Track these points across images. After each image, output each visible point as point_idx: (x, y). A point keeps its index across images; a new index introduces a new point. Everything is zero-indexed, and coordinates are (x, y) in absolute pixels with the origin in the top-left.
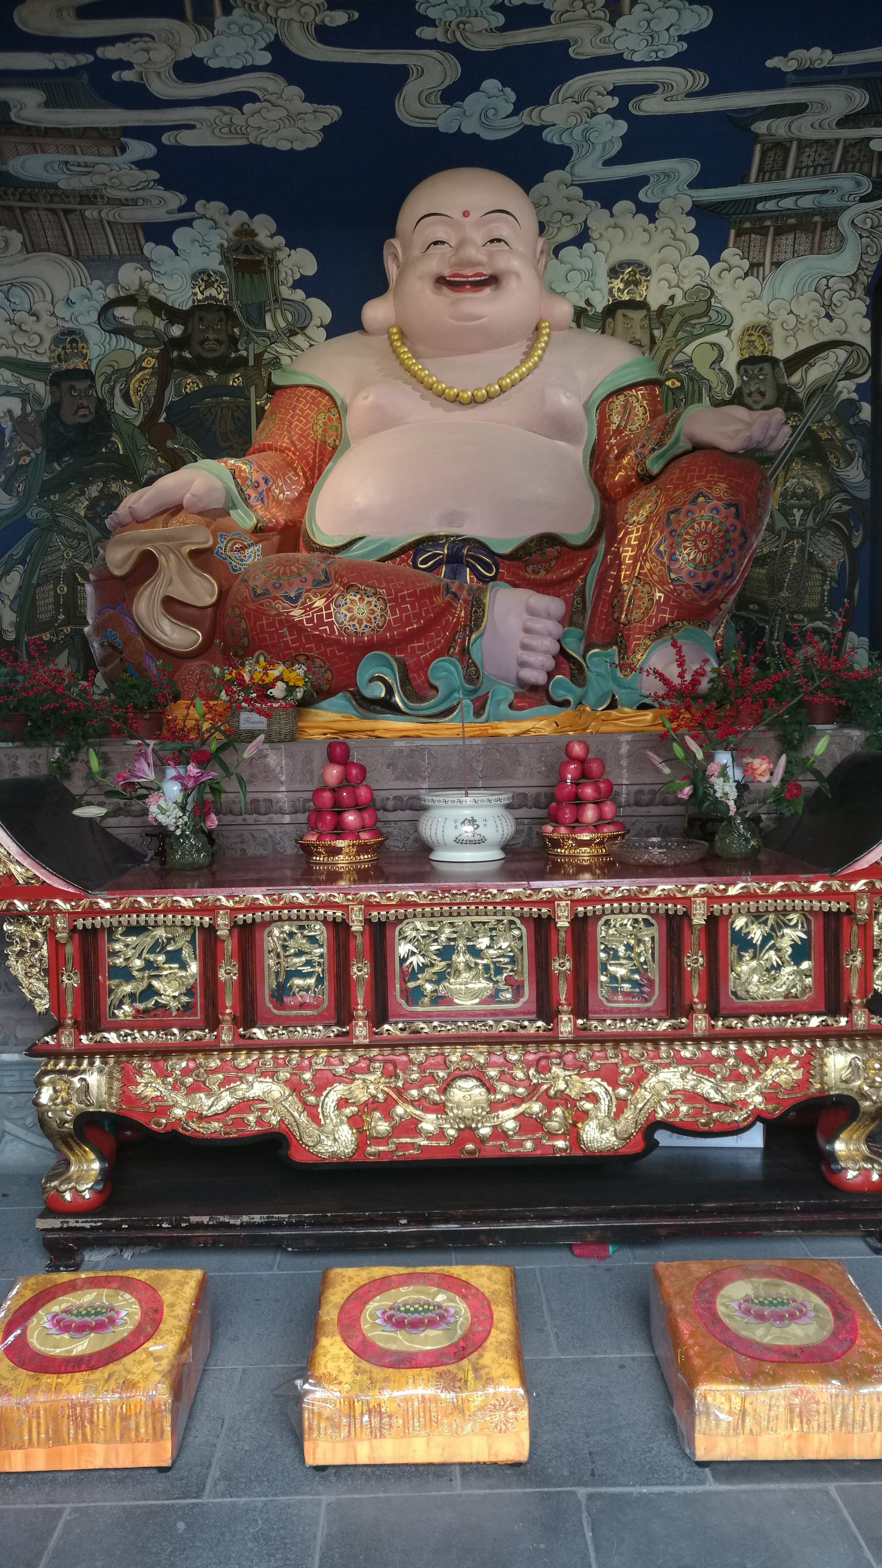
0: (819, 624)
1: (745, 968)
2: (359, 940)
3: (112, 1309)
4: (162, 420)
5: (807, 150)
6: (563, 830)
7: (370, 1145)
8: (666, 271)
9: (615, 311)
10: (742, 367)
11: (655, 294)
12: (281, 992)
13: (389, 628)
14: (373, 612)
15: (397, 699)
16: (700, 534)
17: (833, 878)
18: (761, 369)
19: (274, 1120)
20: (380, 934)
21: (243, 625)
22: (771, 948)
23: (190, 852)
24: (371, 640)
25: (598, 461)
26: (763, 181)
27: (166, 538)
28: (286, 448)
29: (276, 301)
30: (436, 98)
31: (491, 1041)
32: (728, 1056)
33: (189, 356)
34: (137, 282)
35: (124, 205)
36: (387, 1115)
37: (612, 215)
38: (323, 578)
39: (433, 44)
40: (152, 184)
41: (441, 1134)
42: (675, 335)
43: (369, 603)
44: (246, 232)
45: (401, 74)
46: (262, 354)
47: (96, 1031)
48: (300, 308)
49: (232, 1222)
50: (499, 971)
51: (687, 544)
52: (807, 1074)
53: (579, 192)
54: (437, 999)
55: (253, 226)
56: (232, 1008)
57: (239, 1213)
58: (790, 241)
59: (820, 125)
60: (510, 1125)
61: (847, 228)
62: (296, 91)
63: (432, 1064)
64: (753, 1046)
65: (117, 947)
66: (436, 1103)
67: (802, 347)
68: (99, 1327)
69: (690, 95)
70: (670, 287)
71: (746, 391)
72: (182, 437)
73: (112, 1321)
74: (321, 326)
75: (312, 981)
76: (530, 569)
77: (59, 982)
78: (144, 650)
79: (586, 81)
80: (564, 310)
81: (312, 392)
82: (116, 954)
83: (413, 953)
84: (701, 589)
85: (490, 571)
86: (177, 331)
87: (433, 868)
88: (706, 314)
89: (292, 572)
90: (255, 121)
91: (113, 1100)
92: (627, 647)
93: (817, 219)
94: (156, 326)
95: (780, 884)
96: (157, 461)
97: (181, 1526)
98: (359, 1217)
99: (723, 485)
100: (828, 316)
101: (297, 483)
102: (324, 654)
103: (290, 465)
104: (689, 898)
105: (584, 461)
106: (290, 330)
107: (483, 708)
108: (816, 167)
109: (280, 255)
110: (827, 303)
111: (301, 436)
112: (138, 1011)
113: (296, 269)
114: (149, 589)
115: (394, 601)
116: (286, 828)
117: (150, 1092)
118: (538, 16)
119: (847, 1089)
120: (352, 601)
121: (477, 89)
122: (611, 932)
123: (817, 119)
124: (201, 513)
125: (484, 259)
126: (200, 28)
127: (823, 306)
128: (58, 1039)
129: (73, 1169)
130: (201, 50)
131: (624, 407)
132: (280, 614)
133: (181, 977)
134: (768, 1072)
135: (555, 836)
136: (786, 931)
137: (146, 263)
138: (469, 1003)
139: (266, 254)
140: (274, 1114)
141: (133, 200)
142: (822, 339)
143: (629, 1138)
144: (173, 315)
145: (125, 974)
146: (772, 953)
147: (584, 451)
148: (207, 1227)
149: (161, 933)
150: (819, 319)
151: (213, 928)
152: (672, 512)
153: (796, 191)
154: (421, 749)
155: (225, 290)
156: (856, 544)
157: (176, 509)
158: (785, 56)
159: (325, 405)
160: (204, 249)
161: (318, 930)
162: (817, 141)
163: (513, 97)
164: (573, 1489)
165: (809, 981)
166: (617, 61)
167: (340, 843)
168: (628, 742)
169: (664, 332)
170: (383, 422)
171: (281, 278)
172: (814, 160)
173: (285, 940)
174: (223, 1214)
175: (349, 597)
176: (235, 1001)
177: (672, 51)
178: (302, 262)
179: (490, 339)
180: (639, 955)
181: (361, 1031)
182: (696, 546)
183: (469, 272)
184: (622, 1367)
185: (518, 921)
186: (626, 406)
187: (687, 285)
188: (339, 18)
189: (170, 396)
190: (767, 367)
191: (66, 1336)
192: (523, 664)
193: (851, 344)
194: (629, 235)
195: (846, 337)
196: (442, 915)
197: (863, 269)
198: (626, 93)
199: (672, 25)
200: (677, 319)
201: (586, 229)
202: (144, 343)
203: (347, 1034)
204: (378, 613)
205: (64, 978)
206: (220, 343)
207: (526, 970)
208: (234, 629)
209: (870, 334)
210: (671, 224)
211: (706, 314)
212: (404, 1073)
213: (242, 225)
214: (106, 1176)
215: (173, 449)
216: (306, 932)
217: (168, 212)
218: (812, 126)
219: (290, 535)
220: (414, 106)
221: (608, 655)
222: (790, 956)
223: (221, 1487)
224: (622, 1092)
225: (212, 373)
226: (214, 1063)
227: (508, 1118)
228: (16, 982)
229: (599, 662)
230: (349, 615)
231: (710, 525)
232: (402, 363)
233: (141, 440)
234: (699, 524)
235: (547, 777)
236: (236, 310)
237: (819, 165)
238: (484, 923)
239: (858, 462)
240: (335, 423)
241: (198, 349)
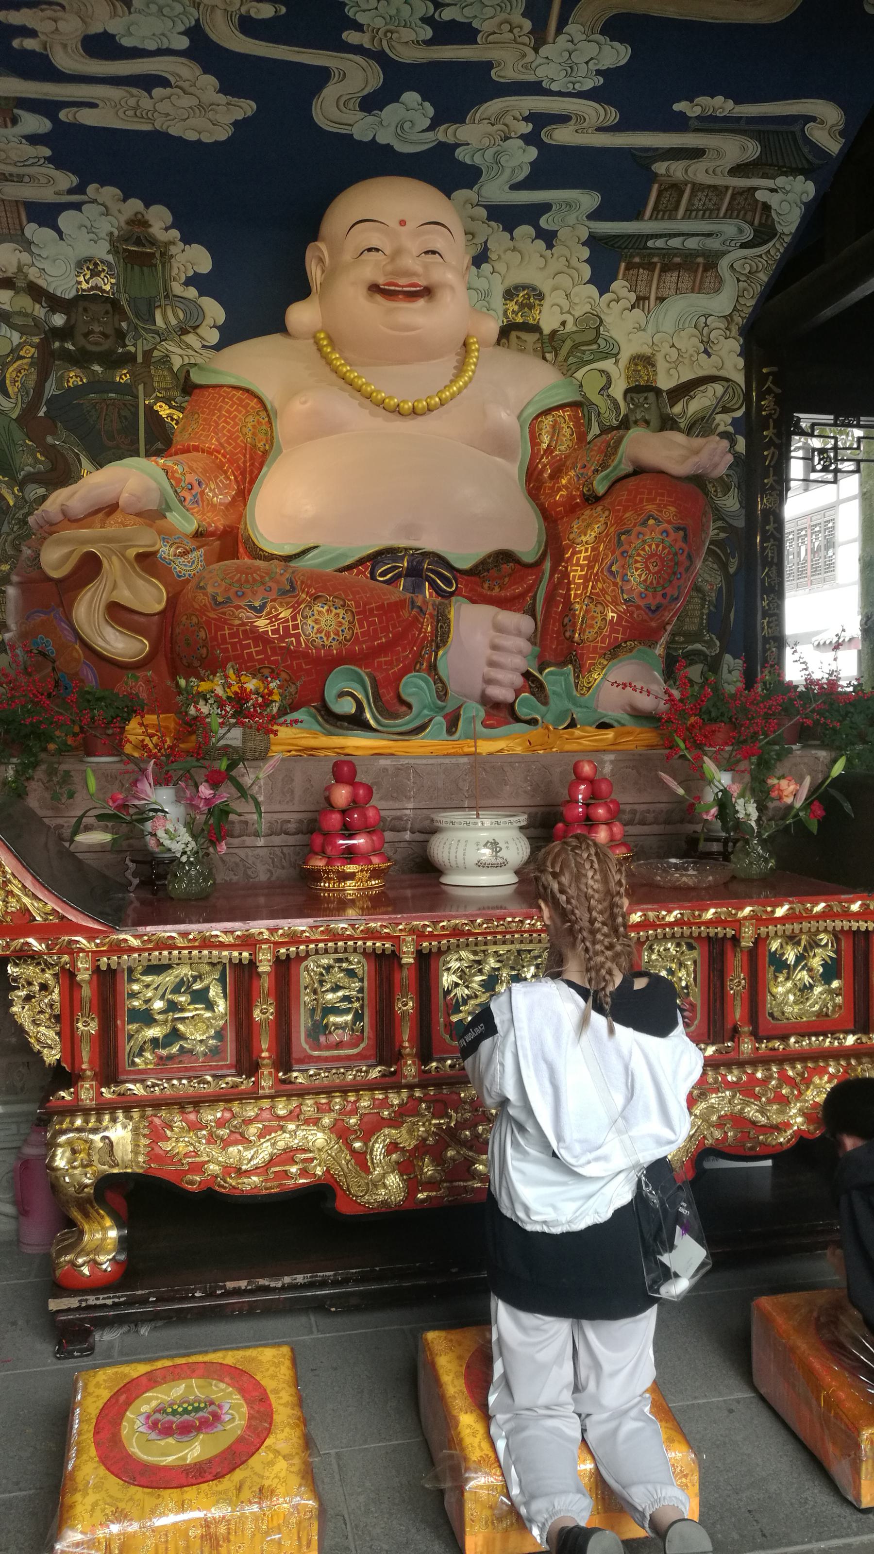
0: (698, 646)
1: (781, 989)
2: (405, 973)
3: (212, 1403)
4: (41, 414)
5: (699, 194)
8: (558, 297)
10: (629, 395)
11: (548, 319)
13: (357, 641)
14: (340, 624)
15: (368, 716)
16: (651, 556)
18: (646, 398)
19: (319, 1171)
20: (427, 963)
21: (202, 634)
22: (803, 969)
23: (197, 881)
24: (339, 653)
25: (534, 483)
26: (656, 219)
28: (215, 450)
30: (354, 104)
32: (771, 1077)
33: (71, 347)
34: (15, 264)
35: (7, 180)
37: (512, 239)
39: (358, 50)
40: (42, 161)
42: (566, 360)
45: (323, 76)
46: (151, 351)
47: (118, 1083)
48: (192, 306)
51: (638, 565)
53: (484, 213)
55: (147, 217)
58: (674, 279)
59: (714, 171)
61: (725, 270)
62: (210, 81)
64: (793, 1068)
65: (136, 987)
67: (683, 380)
69: (600, 129)
70: (562, 313)
71: (632, 418)
72: (64, 434)
73: (216, 1417)
75: (349, 1018)
76: (486, 585)
77: (73, 1030)
78: (82, 659)
79: (504, 104)
80: (492, 327)
81: (239, 394)
82: (133, 995)
83: (457, 985)
84: (649, 608)
85: (450, 586)
86: (58, 320)
87: (444, 892)
88: (595, 341)
89: (255, 580)
93: (700, 260)
94: (36, 313)
95: (823, 905)
96: (36, 458)
99: (673, 509)
100: (706, 351)
102: (290, 667)
104: (739, 921)
105: (519, 478)
106: (182, 329)
108: (705, 211)
109: (173, 250)
110: (705, 339)
111: (229, 438)
112: (161, 1058)
113: (189, 266)
114: (89, 594)
115: (363, 613)
116: (258, 850)
117: (181, 1148)
118: (465, 33)
120: (319, 612)
122: (654, 957)
123: (713, 164)
124: (139, 514)
125: (419, 269)
126: (118, 4)
127: (702, 342)
128: (76, 1093)
129: (86, 1238)
130: (114, 27)
131: (553, 427)
132: (244, 624)
133: (209, 1019)
134: (809, 1093)
137: (27, 245)
139: (158, 247)
141: (18, 176)
142: (701, 373)
144: (55, 303)
145: (146, 1018)
146: (805, 972)
147: (520, 468)
149: (185, 971)
150: (698, 354)
151: (253, 964)
152: (624, 533)
153: (683, 231)
154: (407, 768)
155: (113, 281)
156: (732, 570)
157: (112, 508)
158: (692, 101)
159: (253, 408)
160: (92, 236)
161: (356, 962)
162: (710, 186)
163: (430, 111)
166: (535, 89)
167: (350, 868)
168: (612, 762)
169: (556, 356)
170: (320, 429)
171: (173, 274)
174: (262, 1277)
175: (317, 608)
177: (588, 85)
178: (198, 259)
179: (422, 350)
181: (410, 1069)
183: (402, 282)
184: (731, 1411)
186: (555, 426)
188: (266, 11)
189: (51, 389)
190: (651, 396)
191: (171, 1440)
192: (489, 681)
193: (727, 380)
195: (722, 373)
197: (738, 311)
198: (540, 121)
199: (592, 59)
200: (568, 344)
201: (486, 249)
202: (22, 330)
204: (346, 625)
205: (80, 1025)
206: (105, 336)
208: (183, 642)
209: (743, 372)
210: (567, 252)
211: (595, 341)
213: (136, 214)
214: (123, 1243)
215: (54, 446)
217: (55, 193)
219: (229, 540)
220: (334, 110)
221: (562, 674)
225: (97, 368)
226: (251, 1112)
228: (20, 1030)
229: (554, 679)
230: (316, 627)
231: (660, 548)
232: (336, 371)
233: (18, 435)
234: (650, 546)
235: (533, 796)
236: (123, 302)
238: (529, 951)
239: (734, 492)
240: (264, 427)
241: (82, 341)
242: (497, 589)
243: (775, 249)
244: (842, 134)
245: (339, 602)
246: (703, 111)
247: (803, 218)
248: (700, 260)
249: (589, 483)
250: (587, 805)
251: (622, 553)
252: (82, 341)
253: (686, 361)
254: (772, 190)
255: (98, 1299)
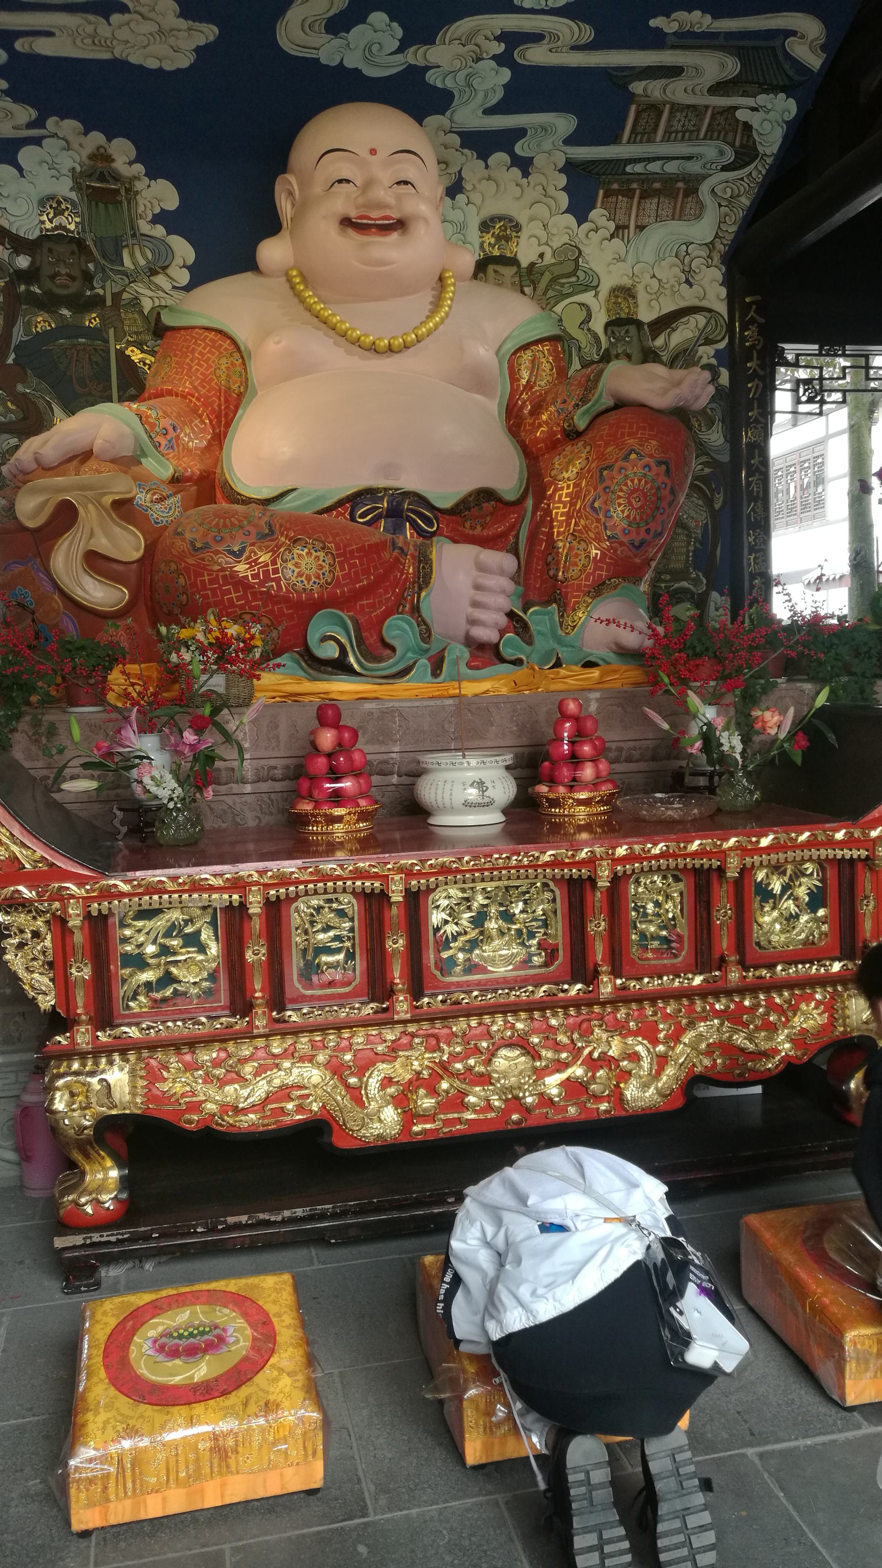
0: (685, 584)
1: (767, 919)
2: (395, 910)
3: (216, 1327)
4: (10, 361)
5: (678, 114)
6: (562, 790)
7: (415, 1124)
8: (535, 228)
9: (487, 266)
11: (526, 251)
12: (311, 969)
13: (338, 584)
14: (321, 567)
15: (352, 660)
16: (634, 491)
17: (854, 826)
18: (627, 332)
19: (315, 1107)
21: (182, 581)
23: (185, 827)
25: (514, 419)
26: (634, 142)
27: (83, 488)
29: (134, 235)
31: (530, 1007)
32: (759, 1005)
33: (38, 291)
36: (433, 1091)
37: (487, 167)
38: (267, 531)
41: (489, 1107)
42: (545, 293)
43: (317, 558)
44: (102, 157)
47: (113, 1026)
49: (273, 1219)
50: (532, 935)
51: (621, 501)
52: (831, 1016)
53: (457, 140)
54: (471, 968)
55: (110, 151)
56: (261, 990)
57: (279, 1209)
58: (654, 206)
59: (693, 90)
60: (554, 1091)
63: (476, 1035)
64: (781, 995)
65: (127, 932)
66: (481, 1075)
67: (665, 311)
68: (211, 1347)
69: (574, 48)
70: (539, 245)
71: (614, 352)
72: (35, 381)
73: (221, 1340)
74: (184, 266)
75: (341, 957)
76: (468, 525)
77: (66, 976)
78: (62, 610)
79: (476, 23)
80: (467, 260)
81: (212, 335)
82: (125, 940)
86: (23, 262)
87: (432, 833)
88: (574, 273)
89: (232, 524)
90: (123, 34)
91: (139, 1100)
92: (565, 605)
93: (680, 185)
97: (362, 1549)
98: (406, 1199)
99: (654, 442)
100: (687, 282)
101: (202, 431)
102: (271, 612)
103: (195, 411)
104: (724, 852)
106: (151, 269)
107: (440, 667)
109: (139, 185)
110: (687, 269)
111: (203, 381)
112: (155, 1001)
113: (155, 202)
115: (343, 555)
116: (246, 798)
117: (178, 1088)
119: (867, 1030)
120: (299, 556)
121: (363, 20)
122: (640, 890)
123: (690, 84)
124: (114, 461)
125: (390, 200)
127: (683, 271)
128: (72, 1038)
129: (88, 1178)
131: (533, 362)
132: (223, 569)
134: (796, 1019)
135: (552, 796)
136: (804, 880)
138: (502, 969)
139: (123, 183)
140: (315, 1101)
142: (683, 304)
143: (670, 1094)
145: (139, 962)
146: (791, 902)
148: (247, 1227)
149: (176, 915)
150: (680, 284)
151: (243, 906)
152: (605, 469)
155: (78, 220)
156: (717, 506)
157: (86, 455)
158: (668, 16)
159: (226, 349)
160: (53, 172)
161: (348, 902)
163: (399, 32)
164: (741, 1451)
165: (825, 928)
167: (339, 811)
168: (597, 700)
169: (535, 289)
170: (296, 369)
171: (140, 211)
172: (683, 126)
173: (312, 915)
174: (263, 1212)
176: (257, 984)
178: (163, 195)
179: (397, 287)
180: (667, 911)
181: (402, 1006)
182: (630, 504)
183: (374, 214)
185: (551, 883)
187: (556, 244)
191: (178, 1362)
192: (473, 622)
193: (710, 311)
194: (502, 187)
195: (704, 304)
196: (473, 881)
197: (720, 238)
198: (513, 40)
200: (547, 277)
203: (385, 1010)
204: (327, 568)
205: (73, 971)
206: (73, 278)
207: (560, 933)
208: (162, 589)
210: (543, 180)
211: (574, 273)
212: (449, 1045)
213: (98, 148)
214: (125, 1183)
215: (24, 394)
216: (335, 905)
218: (685, 90)
219: (207, 486)
222: (807, 904)
223: (383, 1501)
224: (661, 1048)
225: (65, 312)
226: (246, 1051)
227: (553, 1083)
230: (297, 570)
231: (643, 482)
232: (309, 309)
234: (632, 481)
235: (519, 736)
237: (687, 131)
238: (517, 887)
239: (718, 426)
240: (238, 369)
241: (48, 284)
242: (479, 529)
243: (757, 171)
244: (823, 48)
245: (319, 545)
246: (680, 26)
247: (785, 138)
248: (680, 185)
249: (569, 418)
250: (572, 743)
251: (605, 489)
252: (48, 284)
253: (668, 292)
254: (754, 109)
255: (102, 1236)
